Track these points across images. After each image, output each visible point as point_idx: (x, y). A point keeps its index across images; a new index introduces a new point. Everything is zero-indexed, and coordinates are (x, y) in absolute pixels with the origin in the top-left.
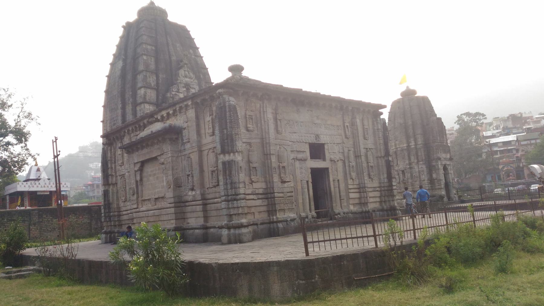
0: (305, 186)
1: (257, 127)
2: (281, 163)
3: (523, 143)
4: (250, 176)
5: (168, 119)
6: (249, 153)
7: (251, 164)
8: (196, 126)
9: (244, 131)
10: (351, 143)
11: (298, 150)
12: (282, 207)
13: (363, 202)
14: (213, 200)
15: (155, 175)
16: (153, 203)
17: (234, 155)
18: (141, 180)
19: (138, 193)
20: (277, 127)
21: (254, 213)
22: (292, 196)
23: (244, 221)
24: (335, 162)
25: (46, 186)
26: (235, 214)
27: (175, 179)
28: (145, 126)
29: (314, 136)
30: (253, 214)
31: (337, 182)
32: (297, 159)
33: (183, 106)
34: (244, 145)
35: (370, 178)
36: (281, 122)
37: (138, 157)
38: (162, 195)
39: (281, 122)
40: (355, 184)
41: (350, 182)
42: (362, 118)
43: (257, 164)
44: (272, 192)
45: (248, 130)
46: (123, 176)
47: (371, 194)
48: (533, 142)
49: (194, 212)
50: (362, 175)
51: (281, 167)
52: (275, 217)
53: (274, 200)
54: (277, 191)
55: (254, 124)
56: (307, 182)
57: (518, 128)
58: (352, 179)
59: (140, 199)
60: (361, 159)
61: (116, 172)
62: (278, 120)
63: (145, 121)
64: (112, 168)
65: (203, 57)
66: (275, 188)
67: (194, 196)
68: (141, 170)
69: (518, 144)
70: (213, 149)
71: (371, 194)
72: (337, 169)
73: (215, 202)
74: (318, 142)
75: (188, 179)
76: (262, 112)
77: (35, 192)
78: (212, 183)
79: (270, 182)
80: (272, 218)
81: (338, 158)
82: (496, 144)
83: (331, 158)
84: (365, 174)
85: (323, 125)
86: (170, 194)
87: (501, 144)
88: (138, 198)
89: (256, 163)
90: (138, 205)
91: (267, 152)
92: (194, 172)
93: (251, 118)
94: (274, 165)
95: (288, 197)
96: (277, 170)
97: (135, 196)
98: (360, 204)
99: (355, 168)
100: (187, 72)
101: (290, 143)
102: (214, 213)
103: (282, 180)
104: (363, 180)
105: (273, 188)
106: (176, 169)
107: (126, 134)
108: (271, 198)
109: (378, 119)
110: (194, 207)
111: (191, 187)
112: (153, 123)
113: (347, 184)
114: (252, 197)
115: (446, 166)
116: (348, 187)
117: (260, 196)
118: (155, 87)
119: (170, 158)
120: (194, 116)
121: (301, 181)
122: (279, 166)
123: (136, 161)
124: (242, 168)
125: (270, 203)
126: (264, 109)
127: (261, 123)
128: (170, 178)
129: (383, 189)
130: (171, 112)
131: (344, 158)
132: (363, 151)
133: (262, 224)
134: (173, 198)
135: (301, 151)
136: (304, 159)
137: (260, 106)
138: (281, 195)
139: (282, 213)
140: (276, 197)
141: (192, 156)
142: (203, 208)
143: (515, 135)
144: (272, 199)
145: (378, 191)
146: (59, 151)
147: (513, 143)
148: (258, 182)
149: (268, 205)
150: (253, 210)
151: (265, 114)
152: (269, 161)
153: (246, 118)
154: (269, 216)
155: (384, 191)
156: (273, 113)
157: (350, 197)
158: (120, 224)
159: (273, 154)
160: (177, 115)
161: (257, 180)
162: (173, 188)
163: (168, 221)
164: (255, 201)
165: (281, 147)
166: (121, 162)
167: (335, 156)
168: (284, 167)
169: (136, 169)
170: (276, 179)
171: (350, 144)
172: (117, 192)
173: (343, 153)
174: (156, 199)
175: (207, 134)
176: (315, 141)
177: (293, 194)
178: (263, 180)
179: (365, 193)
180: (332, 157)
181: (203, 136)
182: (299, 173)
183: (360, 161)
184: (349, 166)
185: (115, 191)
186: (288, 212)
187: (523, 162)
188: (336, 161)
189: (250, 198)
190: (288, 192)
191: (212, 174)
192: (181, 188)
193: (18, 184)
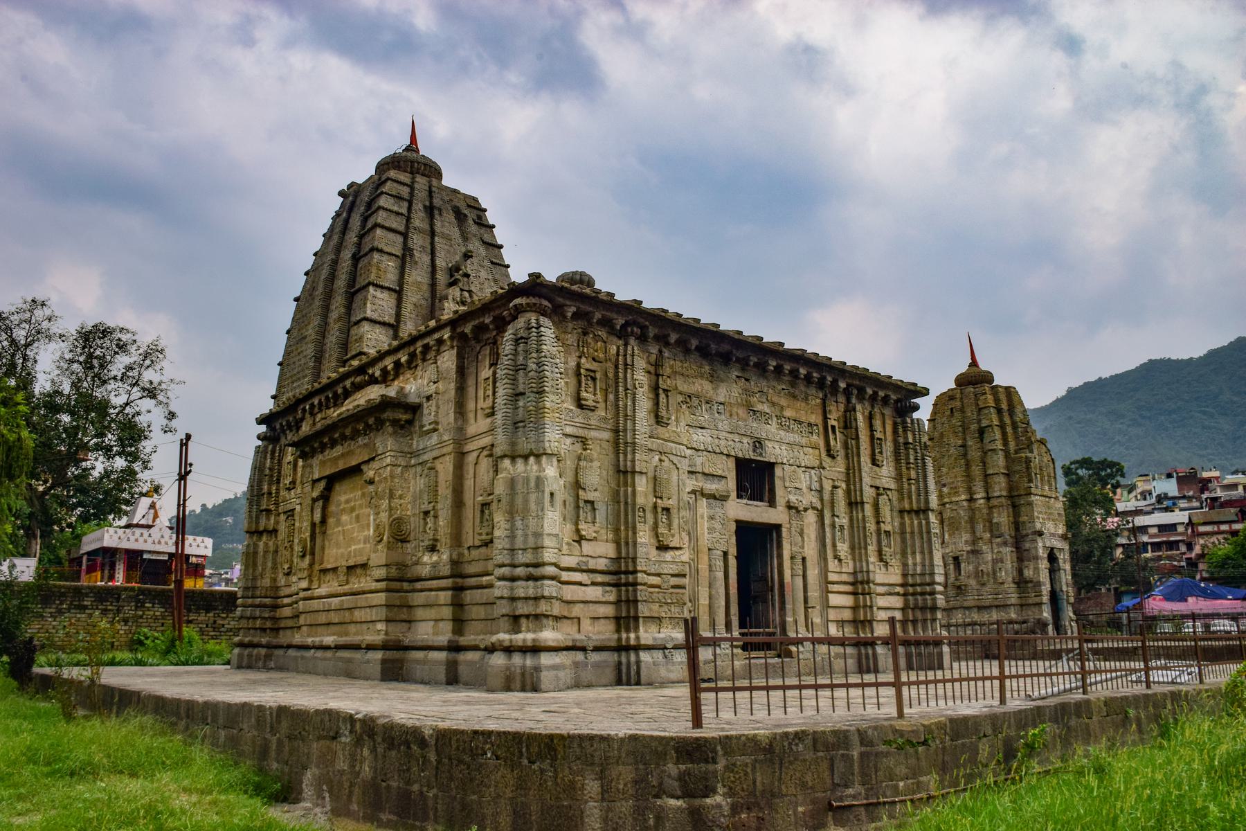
0: (718, 563)
1: (606, 401)
2: (661, 498)
3: (1202, 529)
4: (576, 524)
5: (397, 376)
6: (578, 464)
7: (581, 493)
8: (456, 392)
9: (571, 407)
10: (842, 469)
11: (706, 471)
12: (655, 609)
13: (862, 618)
14: (479, 579)
15: (353, 509)
16: (343, 578)
17: (538, 462)
18: (324, 521)
19: (313, 554)
20: (658, 408)
21: (579, 619)
22: (684, 588)
23: (549, 635)
24: (798, 511)
25: (163, 541)
26: (527, 617)
27: (394, 520)
28: (347, 394)
29: (751, 442)
30: (576, 620)
31: (799, 561)
32: (703, 495)
33: (432, 343)
34: (569, 441)
35: (881, 560)
36: (667, 396)
37: (319, 467)
38: (361, 560)
39: (667, 396)
40: (844, 570)
41: (833, 565)
42: (870, 413)
43: (597, 494)
44: (631, 569)
45: (580, 406)
46: (290, 513)
47: (881, 602)
48: (1224, 527)
49: (431, 606)
50: (863, 551)
51: (659, 510)
52: (632, 635)
53: (635, 591)
54: (645, 569)
55: (598, 392)
56: (725, 554)
57: (1189, 499)
58: (837, 557)
59: (317, 567)
60: (863, 511)
61: (277, 504)
62: (661, 391)
63: (348, 383)
64: (270, 493)
65: (493, 226)
66: (638, 560)
67: (434, 565)
68: (326, 497)
69: (1193, 531)
70: (491, 450)
71: (881, 602)
72: (802, 530)
73: (484, 583)
74: (759, 458)
75: (426, 524)
76: (621, 367)
77: (140, 553)
78: (480, 534)
79: (627, 544)
80: (624, 636)
81: (805, 503)
82: (1144, 529)
83: (788, 502)
84: (872, 549)
85: (775, 419)
86: (379, 557)
87: (1154, 531)
88: (311, 565)
89: (595, 490)
90: (311, 582)
91: (626, 466)
92: (439, 506)
93: (591, 377)
94: (640, 500)
95: (673, 587)
96: (650, 517)
97: (307, 559)
98: (855, 622)
99: (846, 532)
100: (466, 294)
101: (689, 452)
102: (476, 612)
103: (659, 541)
104: (864, 564)
105: (634, 559)
106: (401, 497)
107: (307, 415)
108: (627, 584)
109: (909, 420)
110: (433, 593)
111: (431, 542)
112: (363, 388)
113: (824, 571)
114: (577, 577)
115: (1055, 550)
116: (826, 577)
117: (599, 578)
118: (392, 321)
119: (389, 468)
120: (454, 367)
121: (709, 549)
122: (655, 507)
123: (316, 476)
124: (555, 496)
125: (623, 598)
126: (626, 359)
127: (617, 392)
128: (384, 516)
129: (911, 590)
130: (403, 359)
131: (822, 504)
132: (869, 493)
133: (597, 649)
134: (385, 568)
135: (713, 475)
136: (721, 496)
137: (618, 354)
138: (654, 580)
139: (653, 628)
140: (641, 584)
141: (439, 466)
142: (453, 597)
143: (1187, 513)
144: (630, 588)
145: (898, 594)
146: (191, 465)
147: (1180, 529)
148: (595, 539)
149: (618, 603)
150: (577, 610)
151: (629, 371)
152: (630, 489)
153: (578, 374)
154: (618, 631)
155: (913, 594)
156: (649, 372)
157: (831, 604)
158: (276, 626)
159: (641, 473)
160: (416, 367)
161: (594, 535)
162: (389, 542)
163: (370, 625)
164: (583, 588)
165: (663, 458)
166: (290, 479)
167: (800, 498)
168: (667, 510)
169: (315, 494)
170: (644, 537)
171: (839, 472)
172: (276, 551)
173: (820, 491)
174: (350, 568)
175: (479, 412)
176: (751, 453)
177: (686, 581)
178: (611, 536)
179: (868, 597)
180: (793, 498)
181: (471, 416)
182: (706, 531)
183: (860, 516)
184: (833, 526)
185: (271, 549)
186: (670, 627)
187: (1201, 571)
188: (801, 509)
189: (573, 579)
190: (673, 575)
191: (482, 512)
192: (408, 545)
193: (108, 531)
